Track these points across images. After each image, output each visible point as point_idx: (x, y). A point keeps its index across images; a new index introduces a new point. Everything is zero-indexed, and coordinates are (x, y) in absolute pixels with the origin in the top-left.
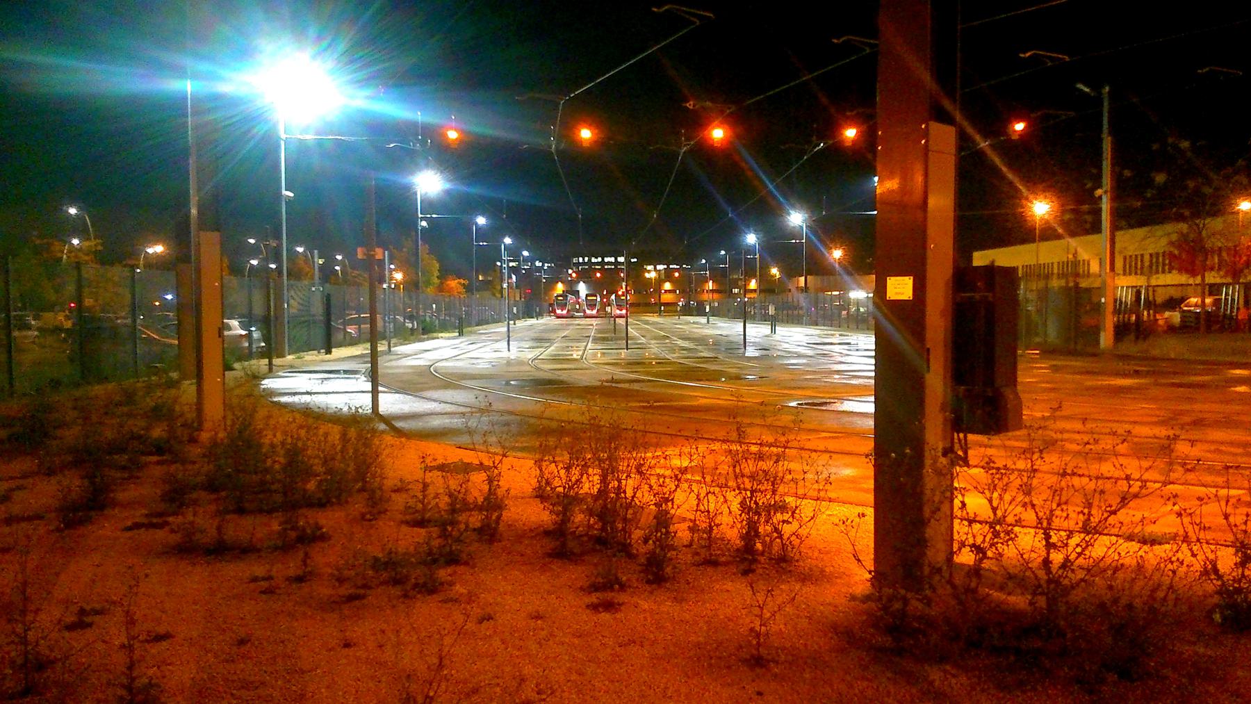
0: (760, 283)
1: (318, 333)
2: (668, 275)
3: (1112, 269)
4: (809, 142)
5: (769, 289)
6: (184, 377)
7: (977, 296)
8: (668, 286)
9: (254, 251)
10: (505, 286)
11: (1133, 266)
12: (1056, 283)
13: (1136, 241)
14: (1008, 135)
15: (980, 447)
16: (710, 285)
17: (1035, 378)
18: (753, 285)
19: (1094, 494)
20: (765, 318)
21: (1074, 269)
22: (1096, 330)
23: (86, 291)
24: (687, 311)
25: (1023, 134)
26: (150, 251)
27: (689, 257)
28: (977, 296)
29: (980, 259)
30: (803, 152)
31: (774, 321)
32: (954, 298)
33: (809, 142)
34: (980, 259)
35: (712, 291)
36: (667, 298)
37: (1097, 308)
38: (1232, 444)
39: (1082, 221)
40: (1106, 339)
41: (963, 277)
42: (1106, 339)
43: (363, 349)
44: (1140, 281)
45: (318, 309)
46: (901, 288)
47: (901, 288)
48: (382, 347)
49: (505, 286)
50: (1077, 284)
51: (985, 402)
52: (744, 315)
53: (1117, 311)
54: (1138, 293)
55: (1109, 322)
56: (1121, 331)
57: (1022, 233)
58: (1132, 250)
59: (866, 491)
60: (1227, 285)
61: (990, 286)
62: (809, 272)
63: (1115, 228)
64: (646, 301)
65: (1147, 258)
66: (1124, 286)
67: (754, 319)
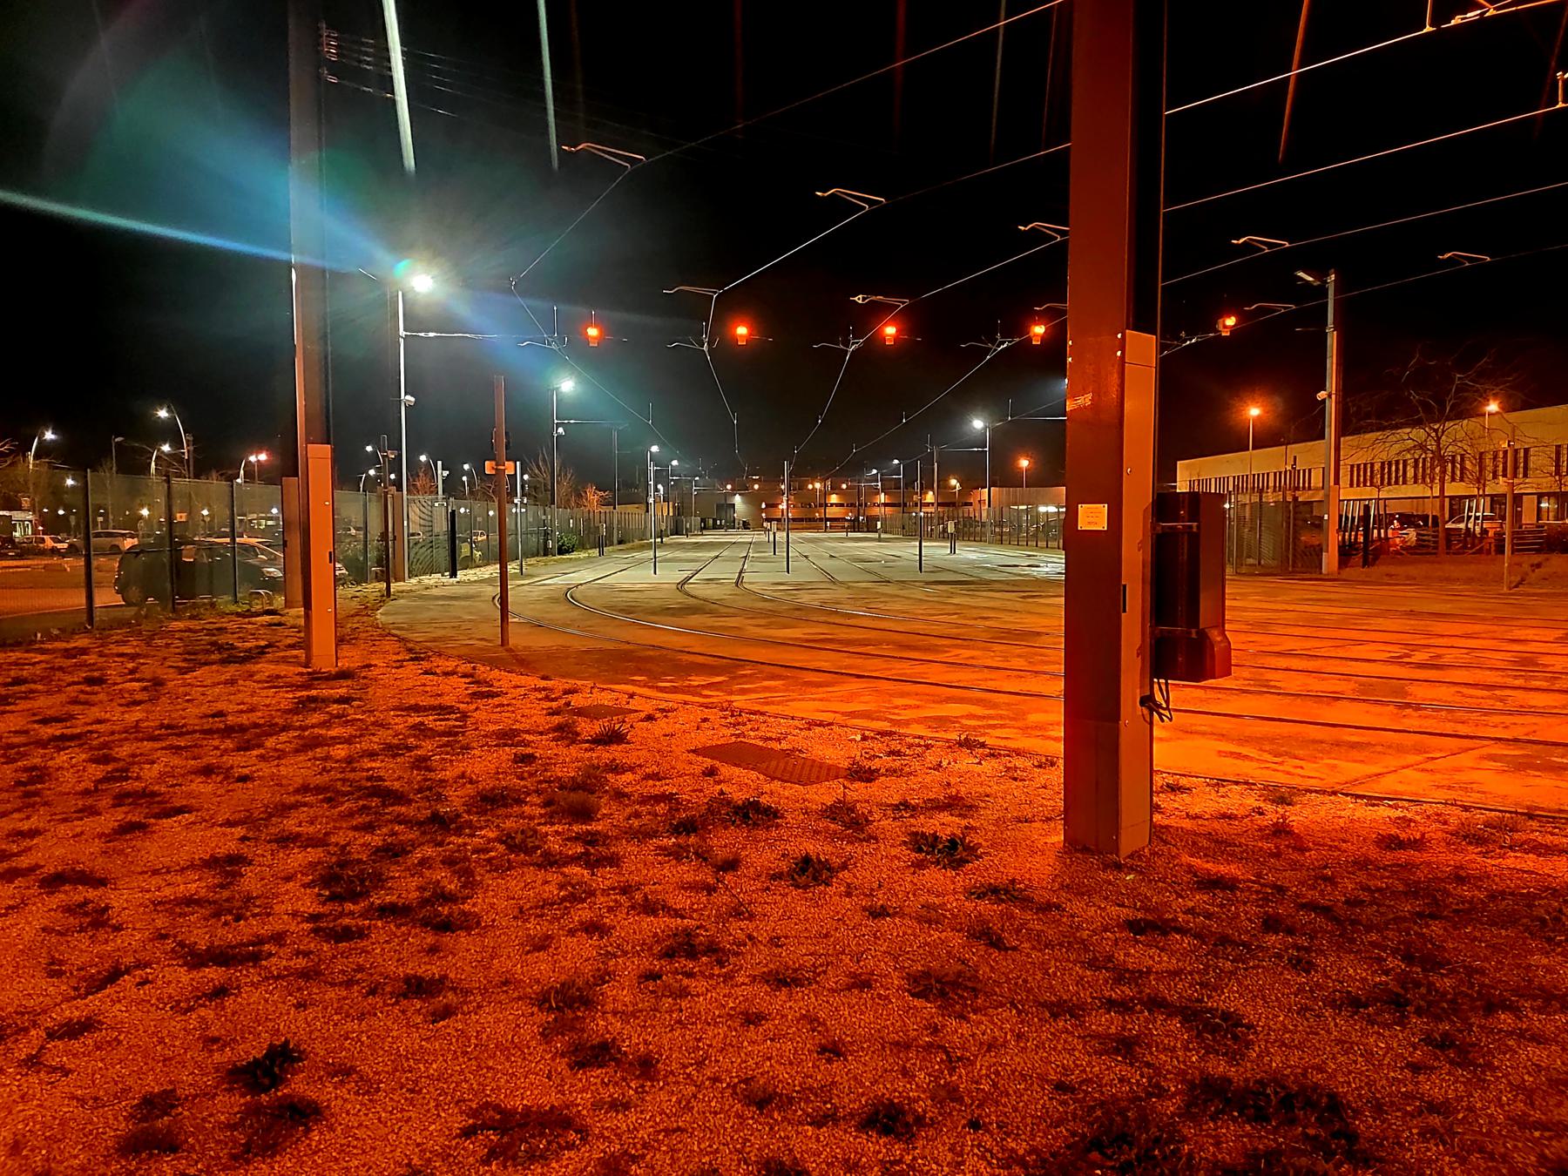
0: (937, 496)
1: (442, 555)
2: (835, 489)
3: (1337, 482)
4: (993, 341)
5: (949, 503)
6: (288, 604)
7: (1180, 525)
8: (834, 499)
9: (373, 460)
10: (651, 500)
11: (1363, 475)
12: (1270, 498)
13: (1366, 449)
14: (1217, 331)
15: (1180, 694)
16: (882, 498)
17: (1248, 608)
18: (930, 497)
19: (1329, 728)
20: (944, 536)
21: (1294, 480)
22: (1318, 551)
23: (177, 502)
24: (855, 526)
25: (1233, 330)
26: (253, 459)
27: (854, 468)
28: (1180, 525)
29: (1186, 476)
30: (987, 351)
31: (953, 539)
32: (1153, 528)
33: (993, 341)
34: (1186, 476)
35: (886, 505)
36: (832, 512)
37: (1319, 525)
38: (1475, 686)
39: (1302, 423)
40: (1330, 559)
41: (1165, 503)
42: (1330, 559)
43: (493, 570)
44: (1369, 492)
45: (442, 526)
46: (1093, 517)
47: (1093, 517)
48: (512, 568)
49: (651, 500)
50: (1295, 499)
51: (1186, 651)
52: (917, 531)
53: (1342, 529)
54: (1367, 508)
55: (1333, 540)
56: (1346, 552)
57: (1233, 442)
58: (1361, 458)
59: (1056, 739)
60: (1470, 497)
61: (1194, 515)
62: (993, 484)
63: (1345, 428)
64: (809, 519)
65: (1377, 467)
66: (1352, 497)
67: (931, 538)
